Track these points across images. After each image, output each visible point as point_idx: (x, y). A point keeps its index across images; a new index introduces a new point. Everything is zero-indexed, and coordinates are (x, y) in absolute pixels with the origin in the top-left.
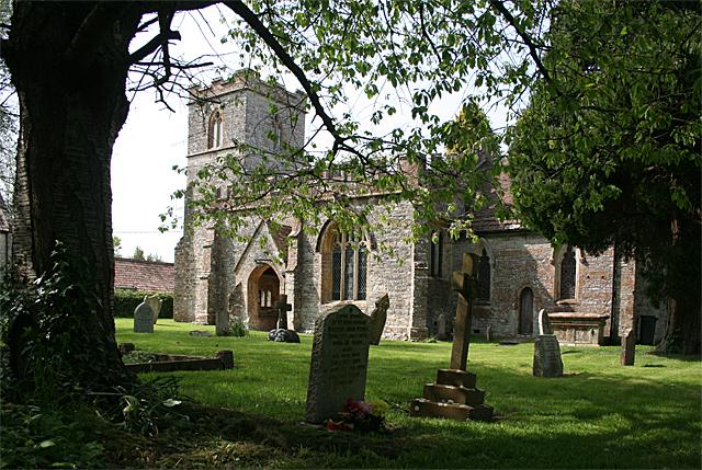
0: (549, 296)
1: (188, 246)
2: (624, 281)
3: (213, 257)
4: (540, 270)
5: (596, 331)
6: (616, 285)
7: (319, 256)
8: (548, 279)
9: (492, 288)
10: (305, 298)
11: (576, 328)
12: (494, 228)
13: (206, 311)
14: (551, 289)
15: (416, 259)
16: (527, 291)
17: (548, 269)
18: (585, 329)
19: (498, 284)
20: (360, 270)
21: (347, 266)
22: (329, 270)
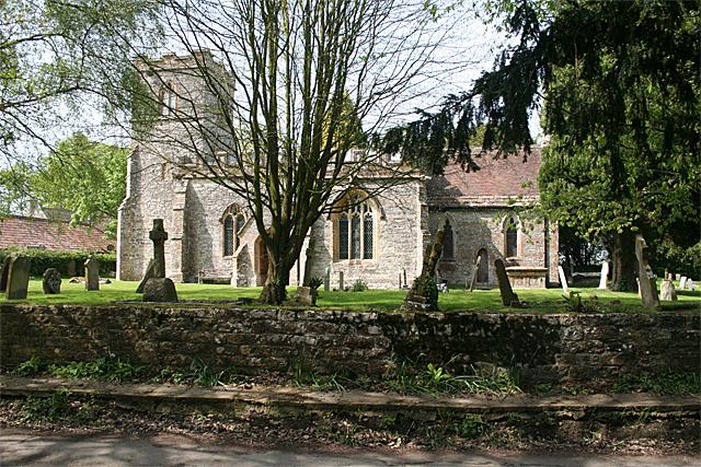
0: (500, 254)
1: (134, 207)
2: (551, 244)
3: (186, 219)
4: (493, 236)
5: (544, 279)
6: (546, 247)
7: (330, 223)
8: (499, 243)
9: (455, 249)
10: (315, 258)
11: (530, 277)
12: (456, 205)
13: (180, 269)
14: (501, 250)
15: (422, 228)
16: (483, 251)
17: (499, 236)
18: (536, 277)
19: (460, 246)
20: (365, 236)
21: (353, 232)
22: (487, 213)
